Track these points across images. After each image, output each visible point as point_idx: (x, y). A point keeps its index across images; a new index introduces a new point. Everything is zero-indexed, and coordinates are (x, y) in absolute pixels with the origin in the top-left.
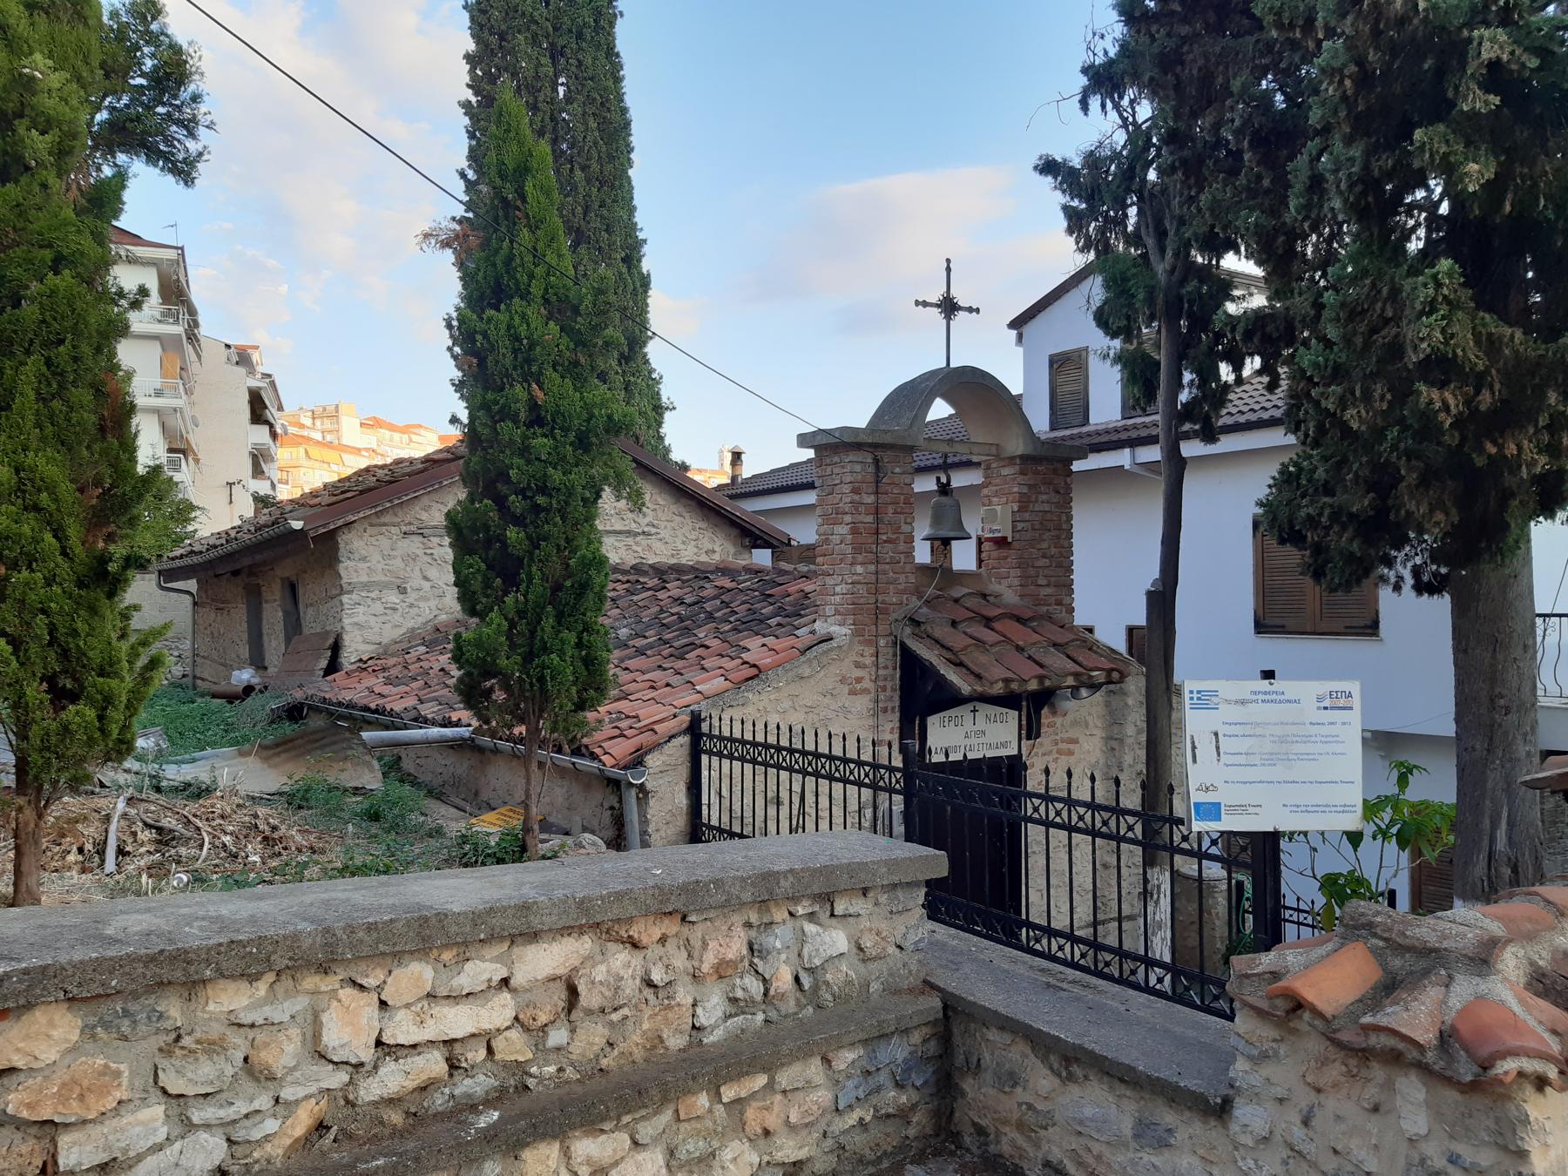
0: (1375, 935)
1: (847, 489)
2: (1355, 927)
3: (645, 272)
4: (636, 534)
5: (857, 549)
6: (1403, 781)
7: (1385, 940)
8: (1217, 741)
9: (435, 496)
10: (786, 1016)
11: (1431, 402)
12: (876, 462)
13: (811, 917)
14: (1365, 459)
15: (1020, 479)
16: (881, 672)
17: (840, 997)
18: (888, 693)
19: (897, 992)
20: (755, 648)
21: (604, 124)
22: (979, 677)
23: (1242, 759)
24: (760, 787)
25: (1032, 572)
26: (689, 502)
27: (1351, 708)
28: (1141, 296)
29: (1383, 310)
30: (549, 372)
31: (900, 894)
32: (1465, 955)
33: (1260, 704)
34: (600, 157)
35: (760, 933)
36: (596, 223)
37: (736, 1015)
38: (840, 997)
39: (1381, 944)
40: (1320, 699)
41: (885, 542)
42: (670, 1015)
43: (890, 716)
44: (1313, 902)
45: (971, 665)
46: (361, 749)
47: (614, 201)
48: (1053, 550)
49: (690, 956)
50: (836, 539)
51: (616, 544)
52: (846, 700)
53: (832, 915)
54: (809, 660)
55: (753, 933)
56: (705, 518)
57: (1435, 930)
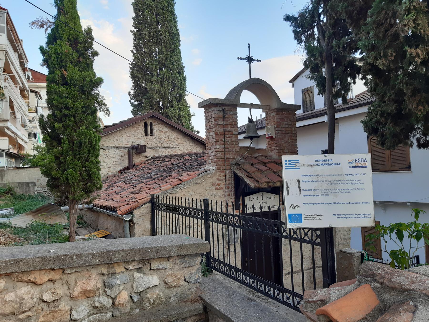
0: (375, 281)
1: (213, 120)
2: (366, 276)
3: (185, 76)
4: (172, 148)
5: (217, 140)
6: (417, 216)
7: (381, 283)
8: (299, 184)
9: (107, 137)
10: (124, 314)
11: (411, 54)
12: (223, 110)
13: (139, 270)
14: (392, 92)
15: (277, 116)
16: (227, 182)
17: (154, 304)
18: (230, 189)
19: (186, 301)
20: (185, 176)
21: (171, 34)
22: (258, 181)
23: (312, 193)
24: (184, 222)
25: (282, 147)
26: (188, 138)
27: (366, 167)
28: (317, 54)
29: (390, 21)
30: (70, 65)
31: (187, 260)
32: (425, 294)
33: (320, 166)
34: (170, 43)
35: (108, 277)
36: (169, 62)
37: (97, 313)
38: (154, 304)
39: (379, 285)
40: (350, 163)
41: (228, 137)
42: (55, 315)
43: (231, 197)
44: (388, 261)
45: (255, 178)
46: (61, 212)
47: (174, 56)
48: (290, 141)
49: (69, 289)
50: (211, 137)
51: (165, 151)
52: (215, 192)
53: (151, 269)
54: (200, 178)
55: (105, 278)
56: (194, 142)
57: (407, 278)
